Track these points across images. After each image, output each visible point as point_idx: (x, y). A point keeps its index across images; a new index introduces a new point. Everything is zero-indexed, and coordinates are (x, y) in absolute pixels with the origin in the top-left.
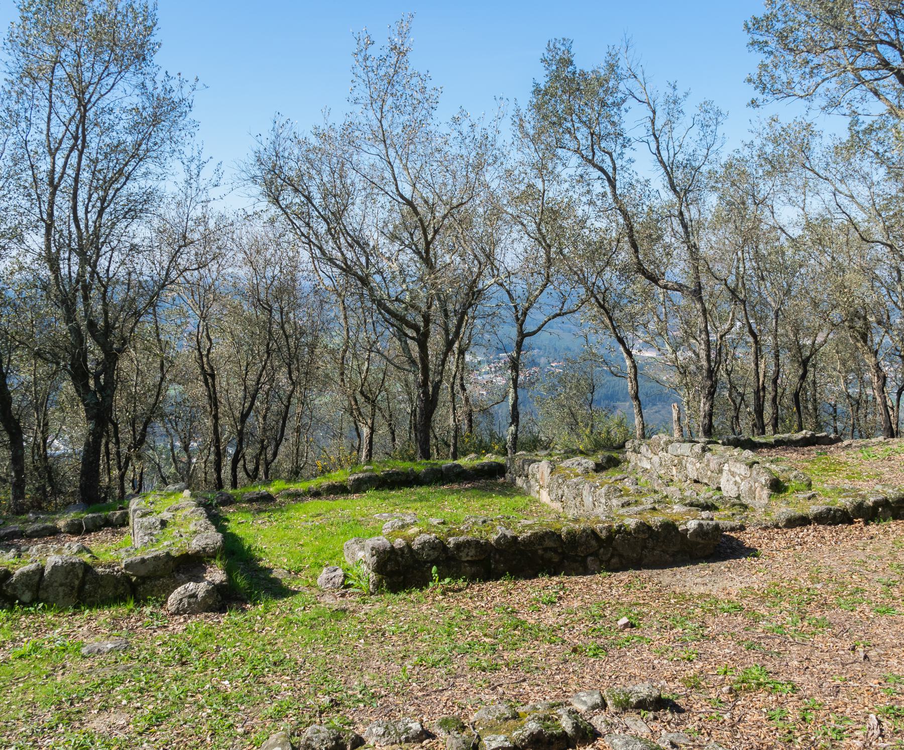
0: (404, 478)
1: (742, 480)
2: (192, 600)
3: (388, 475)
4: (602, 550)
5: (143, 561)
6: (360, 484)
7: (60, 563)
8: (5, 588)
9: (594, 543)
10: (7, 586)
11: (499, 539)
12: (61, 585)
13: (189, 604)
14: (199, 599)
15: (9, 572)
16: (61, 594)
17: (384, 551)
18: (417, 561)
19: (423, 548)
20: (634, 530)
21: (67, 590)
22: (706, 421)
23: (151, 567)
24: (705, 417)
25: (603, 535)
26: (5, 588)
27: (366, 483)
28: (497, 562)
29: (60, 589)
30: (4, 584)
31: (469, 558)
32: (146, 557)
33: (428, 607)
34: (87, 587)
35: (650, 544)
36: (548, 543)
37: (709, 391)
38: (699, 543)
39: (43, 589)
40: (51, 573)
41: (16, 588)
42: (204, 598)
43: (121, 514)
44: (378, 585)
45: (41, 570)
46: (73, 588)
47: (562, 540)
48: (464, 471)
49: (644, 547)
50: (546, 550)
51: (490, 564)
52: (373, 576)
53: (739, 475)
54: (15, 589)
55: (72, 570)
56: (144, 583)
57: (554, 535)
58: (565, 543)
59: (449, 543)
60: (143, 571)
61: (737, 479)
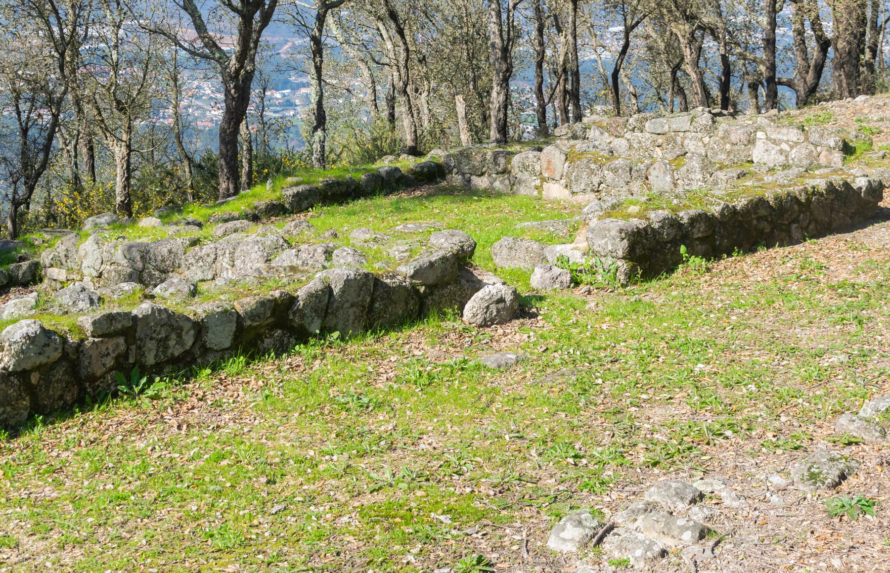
0: (344, 189)
1: (792, 147)
2: (501, 306)
3: (329, 185)
4: (802, 215)
5: (432, 264)
6: (300, 200)
7: (352, 276)
8: (291, 317)
9: (796, 207)
10: (294, 313)
11: (723, 209)
12: (352, 305)
13: (498, 311)
14: (508, 303)
15: (293, 297)
16: (352, 318)
17: (633, 232)
18: (658, 242)
19: (662, 227)
20: (826, 190)
21: (358, 312)
22: (501, 115)
23: (439, 272)
24: (499, 110)
25: (803, 198)
26: (291, 317)
27: (307, 199)
28: (722, 237)
29: (351, 311)
30: (290, 312)
31: (700, 235)
32: (433, 259)
33: (700, 286)
34: (377, 305)
35: (837, 205)
36: (762, 212)
37: (504, 76)
38: (871, 202)
39: (332, 313)
40: (343, 291)
41: (305, 315)
42: (511, 304)
43: (30, 266)
44: (630, 276)
45: (328, 290)
46: (363, 307)
47: (772, 207)
48: (403, 177)
49: (832, 210)
50: (759, 219)
51: (715, 240)
52: (623, 266)
53: (787, 142)
54: (303, 316)
55: (365, 284)
56: (432, 294)
57: (761, 202)
58: (774, 210)
59: (682, 218)
60: (431, 279)
61: (785, 146)
